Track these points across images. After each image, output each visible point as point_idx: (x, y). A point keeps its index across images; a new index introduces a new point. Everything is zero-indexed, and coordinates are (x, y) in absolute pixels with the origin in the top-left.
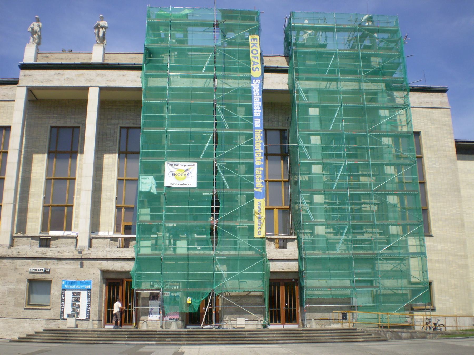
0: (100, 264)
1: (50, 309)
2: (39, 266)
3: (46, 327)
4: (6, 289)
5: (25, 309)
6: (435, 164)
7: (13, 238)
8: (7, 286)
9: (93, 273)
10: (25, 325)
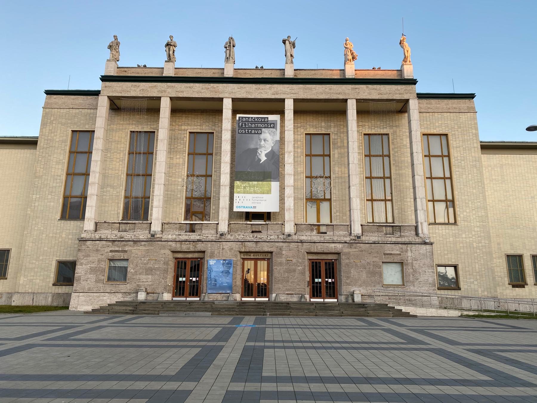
3: (122, 299)
6: (461, 162)
10: (105, 298)
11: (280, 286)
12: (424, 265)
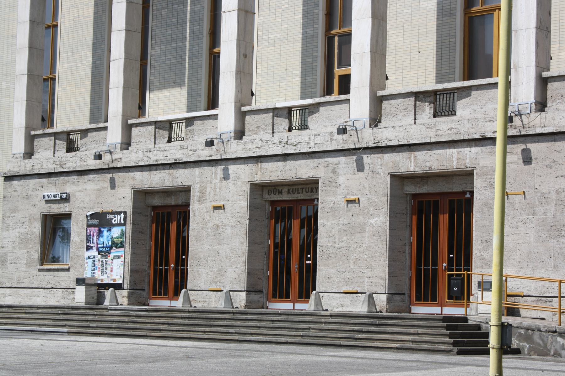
1: (68, 270)
2: (52, 189)
4: (18, 235)
5: (40, 270)
7: (30, 140)
8: (18, 230)
9: (121, 200)
11: (332, 271)
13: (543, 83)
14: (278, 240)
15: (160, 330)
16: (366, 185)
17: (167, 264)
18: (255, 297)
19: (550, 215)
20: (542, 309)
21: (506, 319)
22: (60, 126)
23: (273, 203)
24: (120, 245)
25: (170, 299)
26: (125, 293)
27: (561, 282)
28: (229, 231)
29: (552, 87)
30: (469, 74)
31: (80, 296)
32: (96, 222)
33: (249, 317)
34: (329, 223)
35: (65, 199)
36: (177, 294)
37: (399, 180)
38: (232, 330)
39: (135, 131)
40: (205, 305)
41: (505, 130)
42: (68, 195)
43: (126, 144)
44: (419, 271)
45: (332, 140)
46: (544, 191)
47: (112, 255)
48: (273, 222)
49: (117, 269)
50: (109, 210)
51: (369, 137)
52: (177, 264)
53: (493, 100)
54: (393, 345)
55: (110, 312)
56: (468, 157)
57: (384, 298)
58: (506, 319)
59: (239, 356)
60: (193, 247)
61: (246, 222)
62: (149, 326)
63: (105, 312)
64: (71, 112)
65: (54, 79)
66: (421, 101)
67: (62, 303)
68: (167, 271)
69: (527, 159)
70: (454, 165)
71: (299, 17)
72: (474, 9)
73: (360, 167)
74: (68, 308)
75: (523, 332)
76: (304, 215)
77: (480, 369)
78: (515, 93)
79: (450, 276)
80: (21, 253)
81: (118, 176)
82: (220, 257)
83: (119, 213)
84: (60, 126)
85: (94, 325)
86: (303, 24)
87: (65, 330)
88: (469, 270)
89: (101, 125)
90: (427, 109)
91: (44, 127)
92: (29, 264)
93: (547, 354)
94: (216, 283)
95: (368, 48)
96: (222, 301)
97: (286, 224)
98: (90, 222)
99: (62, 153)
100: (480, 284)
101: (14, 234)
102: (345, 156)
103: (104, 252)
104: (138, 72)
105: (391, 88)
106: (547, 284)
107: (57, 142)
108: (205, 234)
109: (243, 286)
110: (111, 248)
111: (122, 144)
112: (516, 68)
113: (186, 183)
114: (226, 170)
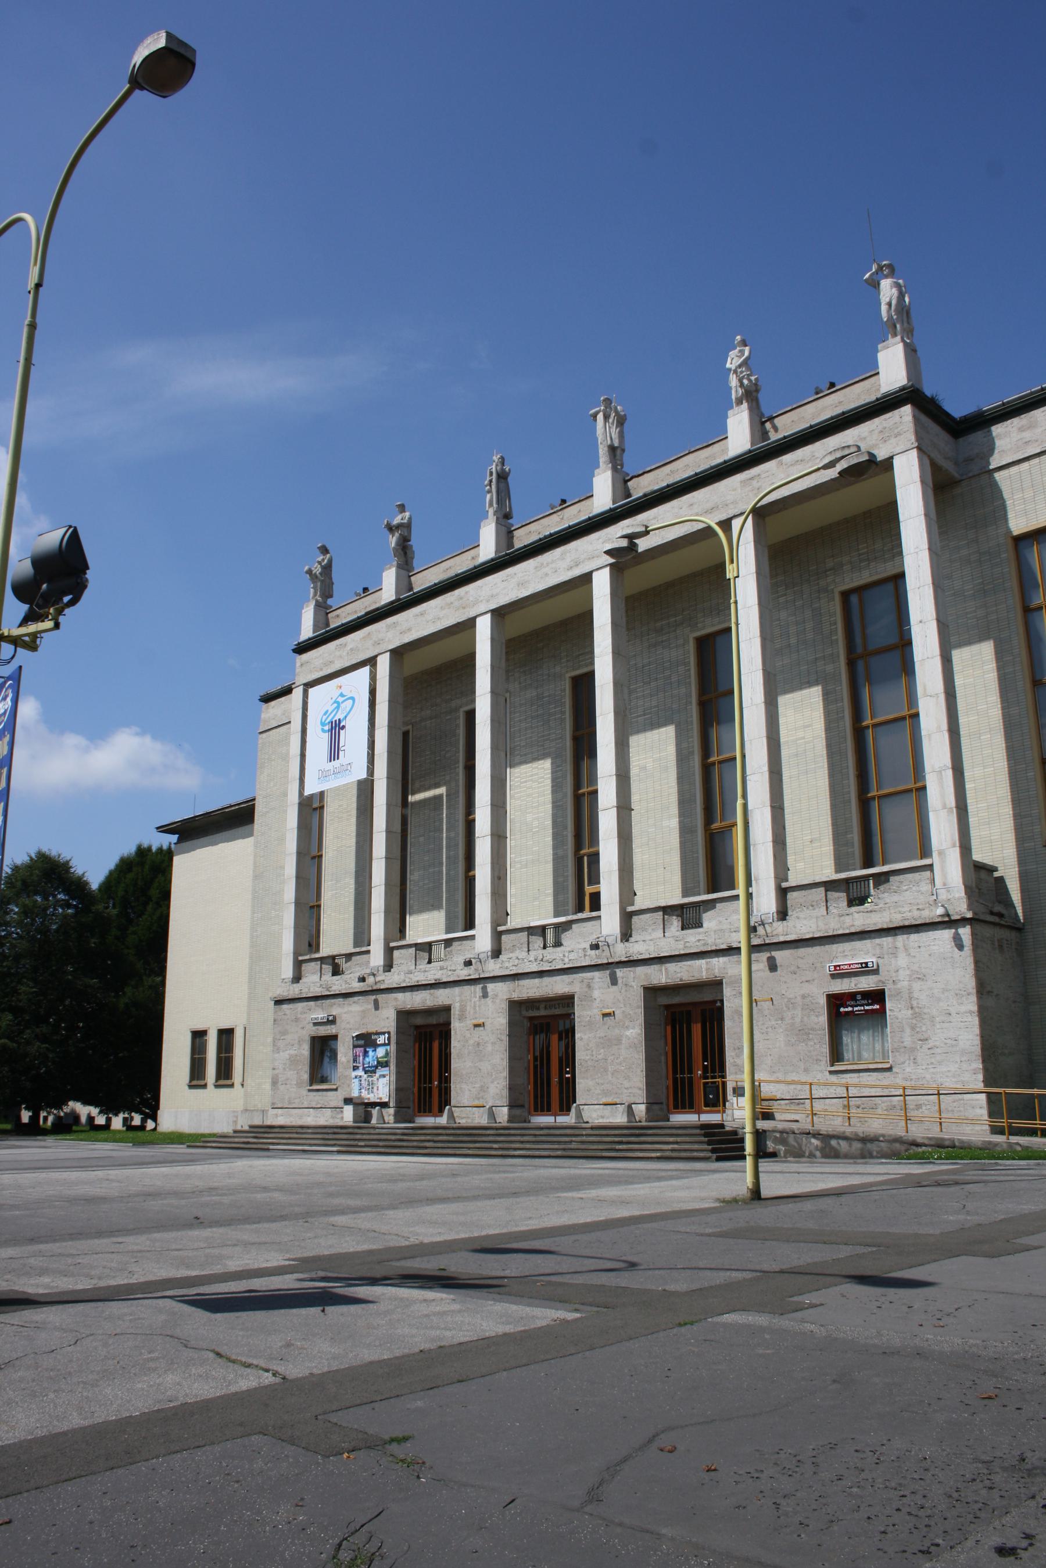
0: (396, 999)
1: (336, 1090)
5: (310, 1090)
7: (298, 965)
9: (385, 1020)
11: (591, 1083)
12: (944, 990)
13: (783, 893)
14: (538, 1054)
15: (426, 1148)
16: (621, 998)
17: (431, 1082)
18: (517, 1112)
19: (798, 1020)
20: (796, 1112)
21: (762, 1125)
22: (325, 951)
23: (531, 1019)
24: (386, 1064)
25: (435, 1116)
26: (391, 1111)
27: (811, 1084)
28: (489, 1048)
29: (791, 896)
30: (713, 888)
31: (348, 1114)
32: (362, 1042)
33: (512, 1132)
34: (586, 1037)
35: (332, 1021)
36: (441, 1111)
37: (651, 992)
38: (495, 1146)
39: (396, 953)
40: (469, 1121)
41: (749, 939)
42: (335, 1017)
43: (388, 966)
44: (675, 1080)
45: (585, 955)
46: (791, 996)
47: (377, 1075)
48: (532, 1037)
49: (382, 1088)
50: (374, 1030)
51: (621, 951)
52: (440, 1082)
53: (737, 911)
54: (653, 1155)
55: (377, 1131)
56: (717, 966)
57: (643, 1107)
58: (762, 1125)
59: (504, 1172)
60: (455, 1064)
61: (505, 1039)
62: (415, 1144)
63: (372, 1131)
64: (336, 936)
65: (319, 906)
66: (670, 915)
67: (331, 1122)
68: (430, 1088)
69: (773, 966)
70: (704, 976)
71: (549, 839)
72: (714, 826)
73: (614, 981)
74: (337, 1127)
75: (778, 1135)
76: (561, 1028)
77: (739, 1174)
78: (757, 903)
79: (705, 1084)
80: (291, 1074)
81: (381, 997)
82: (481, 1076)
83: (384, 1033)
84: (325, 951)
85: (362, 1144)
86: (554, 845)
87: (335, 1149)
88: (724, 1077)
89: (364, 949)
90: (675, 923)
91: (311, 952)
92: (299, 1085)
93: (802, 1156)
94: (478, 1099)
95: (616, 867)
96: (486, 1117)
97: (544, 1037)
98: (356, 1043)
99: (328, 977)
100: (734, 1090)
101: (285, 1055)
102: (598, 970)
103: (370, 1071)
104: (398, 898)
105: (640, 903)
106: (799, 1087)
107: (324, 966)
108: (466, 1052)
109: (505, 1101)
110: (376, 1067)
111: (384, 966)
112: (756, 880)
113: (447, 1002)
114: (484, 989)
